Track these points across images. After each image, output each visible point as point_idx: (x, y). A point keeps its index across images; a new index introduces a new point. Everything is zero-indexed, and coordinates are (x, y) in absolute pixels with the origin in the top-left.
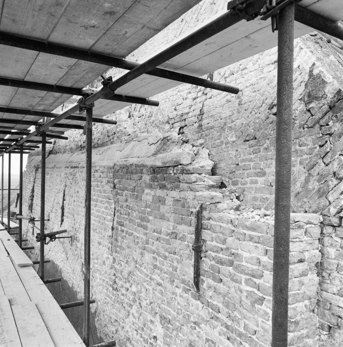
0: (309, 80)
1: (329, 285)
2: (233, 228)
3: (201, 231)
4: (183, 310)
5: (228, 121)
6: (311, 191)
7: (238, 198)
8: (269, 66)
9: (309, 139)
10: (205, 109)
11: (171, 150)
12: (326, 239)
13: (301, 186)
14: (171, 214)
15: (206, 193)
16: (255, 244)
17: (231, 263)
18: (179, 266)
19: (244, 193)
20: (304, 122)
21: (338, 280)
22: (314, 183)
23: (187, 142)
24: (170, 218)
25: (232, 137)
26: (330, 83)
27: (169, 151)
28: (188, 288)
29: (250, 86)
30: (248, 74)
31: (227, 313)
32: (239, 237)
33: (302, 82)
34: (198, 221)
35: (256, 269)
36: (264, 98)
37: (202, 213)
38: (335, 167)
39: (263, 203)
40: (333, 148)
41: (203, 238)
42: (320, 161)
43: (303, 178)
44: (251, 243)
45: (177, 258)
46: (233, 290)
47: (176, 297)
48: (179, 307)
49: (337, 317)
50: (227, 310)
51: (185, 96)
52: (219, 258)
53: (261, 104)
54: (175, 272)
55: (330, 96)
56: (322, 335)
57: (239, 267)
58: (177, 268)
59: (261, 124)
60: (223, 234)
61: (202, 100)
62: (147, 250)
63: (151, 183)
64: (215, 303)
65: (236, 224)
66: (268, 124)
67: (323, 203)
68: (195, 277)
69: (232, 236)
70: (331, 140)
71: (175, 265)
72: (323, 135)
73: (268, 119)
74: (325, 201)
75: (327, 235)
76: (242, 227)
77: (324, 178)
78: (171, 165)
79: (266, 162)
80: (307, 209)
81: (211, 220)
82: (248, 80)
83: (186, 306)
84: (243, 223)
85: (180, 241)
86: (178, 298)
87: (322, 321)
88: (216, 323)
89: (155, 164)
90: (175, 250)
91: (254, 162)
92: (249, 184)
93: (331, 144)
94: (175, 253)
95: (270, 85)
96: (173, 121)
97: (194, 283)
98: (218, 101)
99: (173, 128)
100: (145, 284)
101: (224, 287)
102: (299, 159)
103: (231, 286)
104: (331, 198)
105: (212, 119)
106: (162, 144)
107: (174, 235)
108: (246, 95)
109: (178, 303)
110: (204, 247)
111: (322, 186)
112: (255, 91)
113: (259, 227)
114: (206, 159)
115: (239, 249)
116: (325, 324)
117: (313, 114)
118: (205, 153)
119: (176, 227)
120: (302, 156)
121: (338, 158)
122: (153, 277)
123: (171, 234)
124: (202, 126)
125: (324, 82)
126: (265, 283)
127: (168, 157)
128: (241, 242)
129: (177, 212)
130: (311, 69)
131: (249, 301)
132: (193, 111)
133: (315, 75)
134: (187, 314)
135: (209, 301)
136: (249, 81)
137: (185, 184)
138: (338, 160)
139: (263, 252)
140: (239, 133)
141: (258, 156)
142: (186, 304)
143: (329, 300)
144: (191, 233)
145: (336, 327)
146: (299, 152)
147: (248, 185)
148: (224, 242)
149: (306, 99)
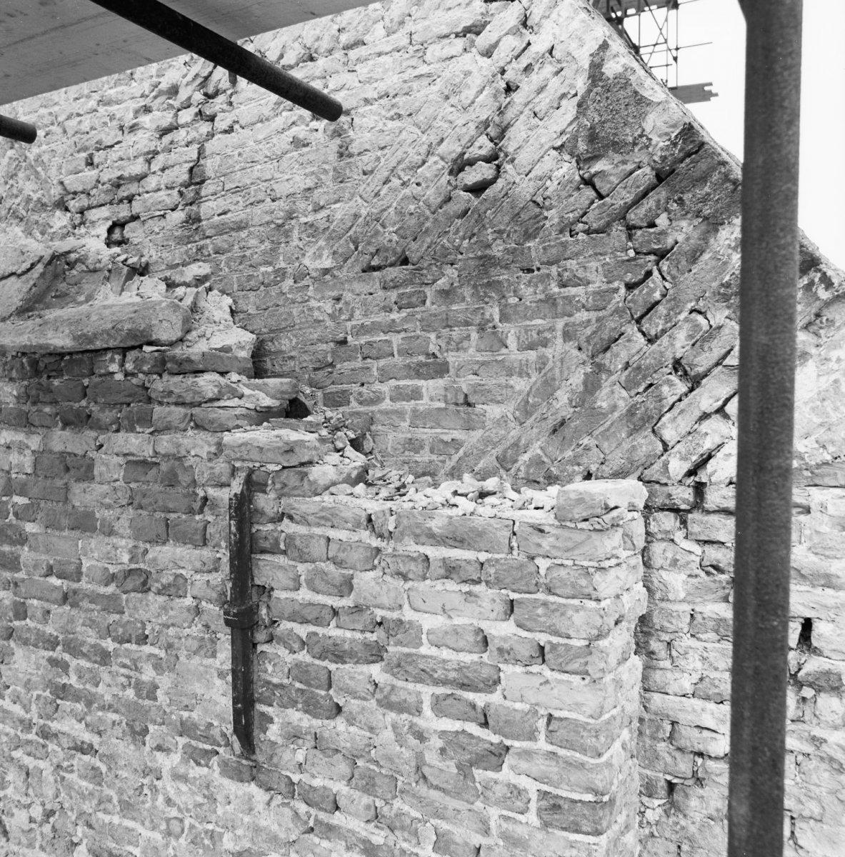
0: (589, 91)
1: (669, 675)
2: (376, 543)
3: (250, 559)
4: (187, 822)
5: (301, 205)
6: (605, 415)
7: (356, 444)
8: (446, 41)
9: (593, 264)
10: (210, 166)
11: (89, 298)
12: (657, 548)
13: (571, 401)
14: (119, 510)
15: (263, 435)
16: (466, 588)
17: (376, 654)
18: (165, 681)
19: (373, 428)
20: (576, 214)
21: (697, 657)
22: (613, 392)
23: (143, 270)
24: (117, 526)
25: (320, 256)
26: (659, 104)
27: (82, 298)
28: (208, 747)
29: (381, 98)
30: (370, 63)
31: (368, 807)
32: (403, 569)
33: (563, 96)
34: (240, 528)
35: (473, 663)
36: (434, 139)
37: (250, 502)
38: (678, 344)
39: (441, 458)
40: (671, 292)
41: (257, 582)
42: (631, 329)
43: (577, 379)
44: (451, 585)
45: (151, 655)
46: (388, 735)
47: (159, 784)
48: (174, 813)
49: (692, 756)
50: (366, 800)
51: (129, 120)
52: (331, 642)
53: (423, 157)
54: (147, 702)
55: (660, 143)
56: (648, 810)
57: (410, 664)
58: (156, 687)
59: (427, 219)
60: (338, 563)
61: (193, 134)
62: (20, 638)
63: (25, 408)
64: (317, 782)
65: (391, 528)
66: (450, 220)
67: (644, 449)
68: (237, 713)
69: (374, 568)
70: (665, 268)
71: (144, 678)
72: (637, 253)
73: (451, 204)
74: (651, 443)
75: (659, 536)
76: (417, 536)
77: (644, 377)
78: (112, 344)
79: (445, 332)
80: (593, 468)
81: (286, 520)
82: (369, 81)
83: (200, 805)
84: (418, 525)
85: (161, 599)
86: (168, 785)
87: (649, 772)
88: (325, 844)
89: (42, 341)
90: (144, 629)
91: (403, 335)
92: (388, 401)
93: (664, 278)
94: (143, 640)
95: (453, 100)
96: (84, 201)
97: (236, 731)
98: (258, 142)
99: (80, 224)
100: (17, 754)
101: (352, 729)
102: (560, 324)
103: (381, 725)
104: (669, 434)
105: (240, 199)
106: (48, 276)
107: (139, 580)
108: (366, 126)
109: (169, 801)
110: (264, 611)
111: (639, 399)
112: (399, 116)
113: (481, 534)
114: (227, 327)
115: (406, 606)
116: (658, 780)
117: (603, 192)
118: (221, 308)
119: (146, 551)
120: (570, 315)
121: (686, 320)
122: (55, 726)
123: (121, 576)
124: (199, 220)
125: (640, 101)
126: (508, 703)
127: (94, 318)
128: (410, 584)
129: (145, 501)
130: (597, 60)
131: (452, 764)
132: (163, 170)
133: (611, 77)
134: (206, 832)
135: (295, 778)
136: (375, 85)
137: (173, 408)
138: (687, 326)
139: (500, 608)
140: (342, 245)
141: (419, 316)
142: (200, 799)
143: (671, 713)
144: (205, 569)
145: (690, 782)
146: (560, 302)
147: (387, 404)
148: (346, 586)
149: (582, 146)
